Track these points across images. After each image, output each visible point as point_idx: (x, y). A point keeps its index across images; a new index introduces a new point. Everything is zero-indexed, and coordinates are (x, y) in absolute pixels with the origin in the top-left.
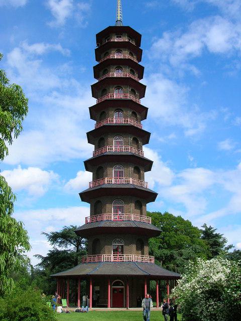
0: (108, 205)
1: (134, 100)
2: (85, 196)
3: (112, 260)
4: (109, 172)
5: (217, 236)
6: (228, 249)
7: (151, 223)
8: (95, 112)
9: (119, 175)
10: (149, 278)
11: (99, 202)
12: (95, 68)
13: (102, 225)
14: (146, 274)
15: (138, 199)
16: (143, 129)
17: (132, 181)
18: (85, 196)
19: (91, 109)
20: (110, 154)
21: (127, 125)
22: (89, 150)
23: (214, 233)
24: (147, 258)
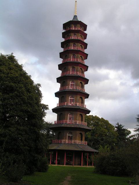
0: (70, 55)
1: (81, 40)
2: (57, 95)
3: (67, 143)
4: (68, 83)
5: (124, 130)
6: (130, 137)
7: (86, 125)
8: (63, 45)
9: (75, 27)
10: (84, 152)
11: (61, 114)
12: (63, 33)
13: (63, 126)
14: (82, 150)
15: (81, 96)
16: (85, 64)
17: (79, 89)
18: (57, 95)
19: (62, 43)
20: (68, 90)
21: (77, 62)
22: (59, 73)
23: (123, 128)
24: (84, 142)
